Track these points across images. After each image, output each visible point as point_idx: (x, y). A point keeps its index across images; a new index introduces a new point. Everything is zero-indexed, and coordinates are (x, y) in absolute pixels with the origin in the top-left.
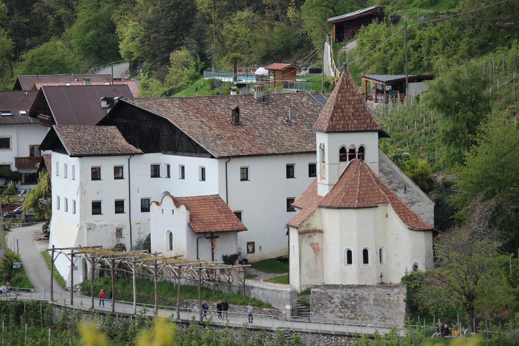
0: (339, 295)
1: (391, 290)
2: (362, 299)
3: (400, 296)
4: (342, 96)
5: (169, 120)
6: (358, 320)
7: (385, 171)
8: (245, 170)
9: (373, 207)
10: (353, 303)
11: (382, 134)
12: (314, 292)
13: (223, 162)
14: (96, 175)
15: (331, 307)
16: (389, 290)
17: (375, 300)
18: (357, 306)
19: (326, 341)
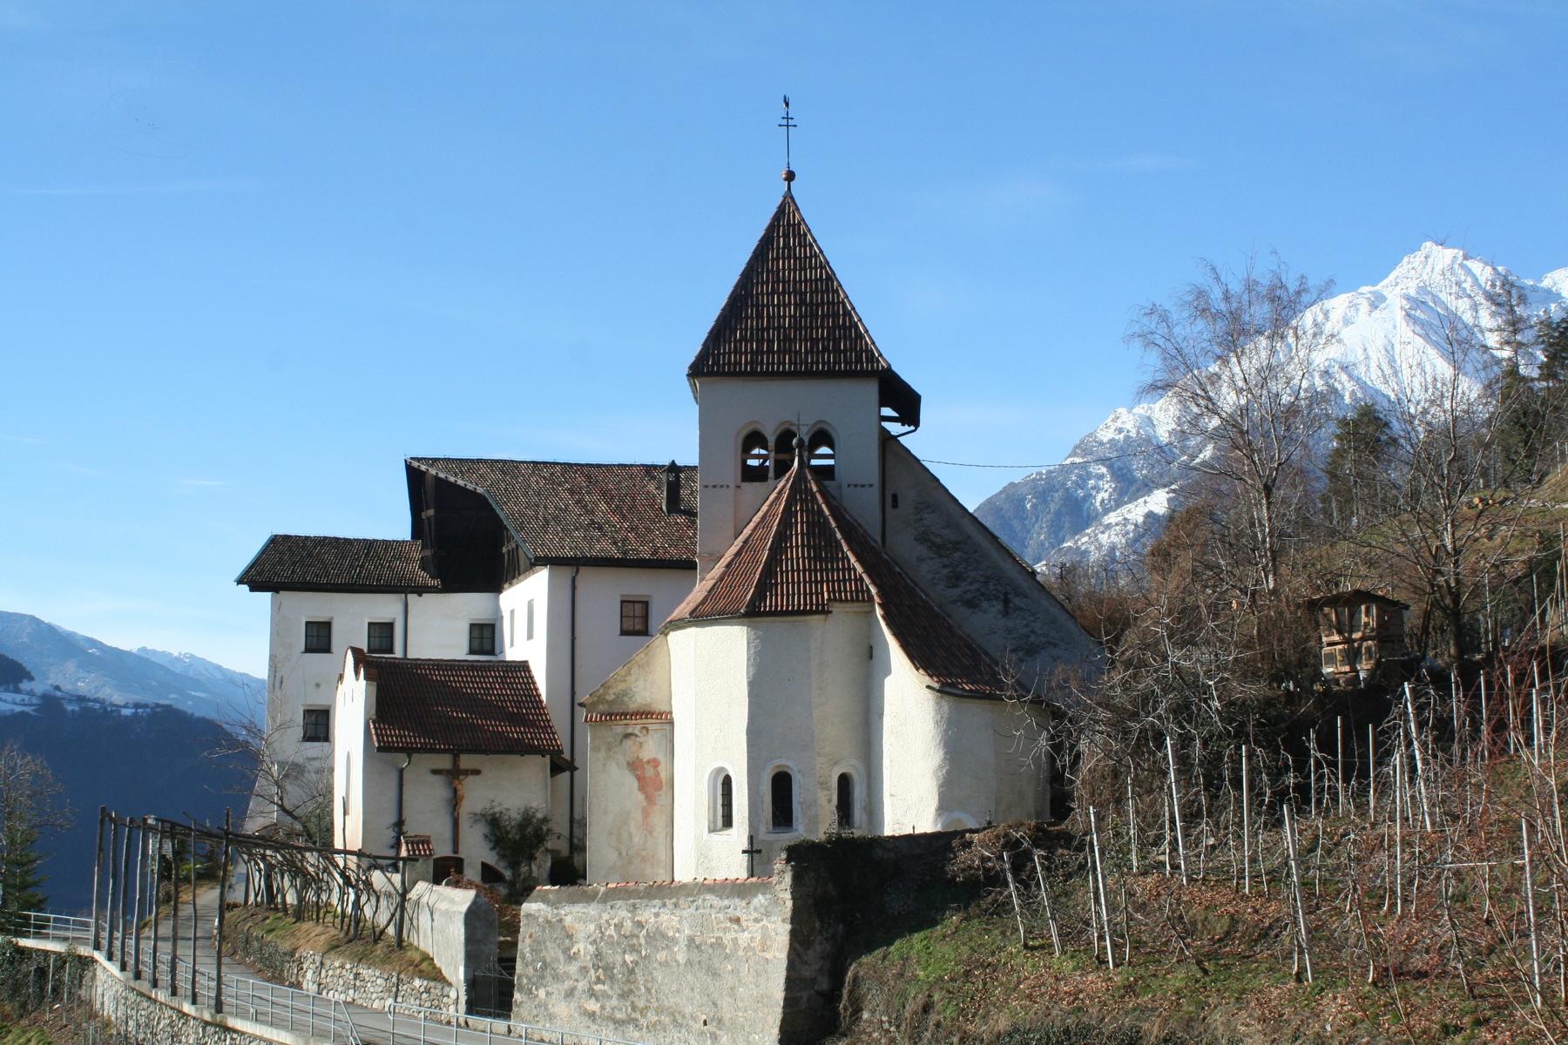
1: (744, 903)
7: (938, 541)
8: (638, 609)
10: (628, 958)
12: (528, 916)
13: (566, 573)
14: (319, 638)
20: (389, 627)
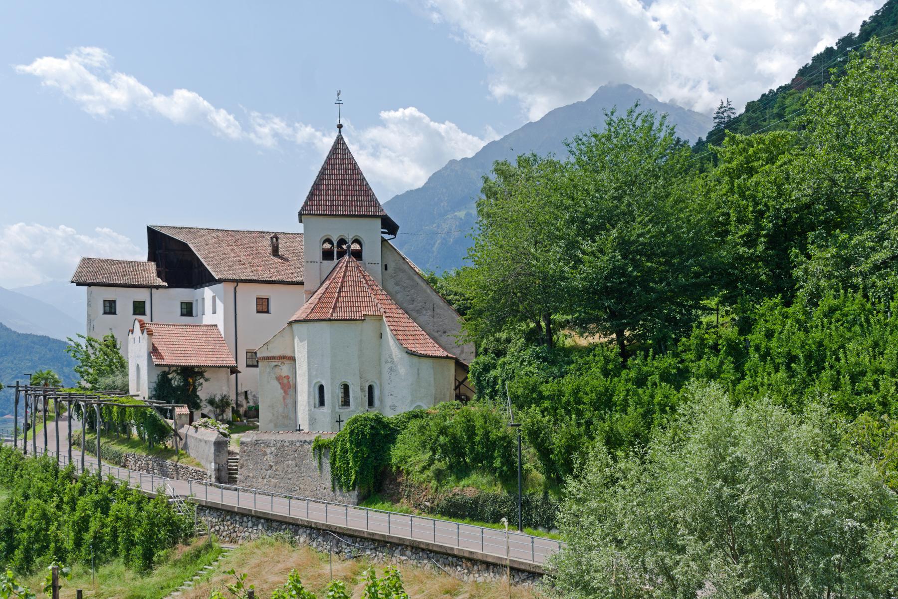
5: (191, 246)
20: (143, 303)
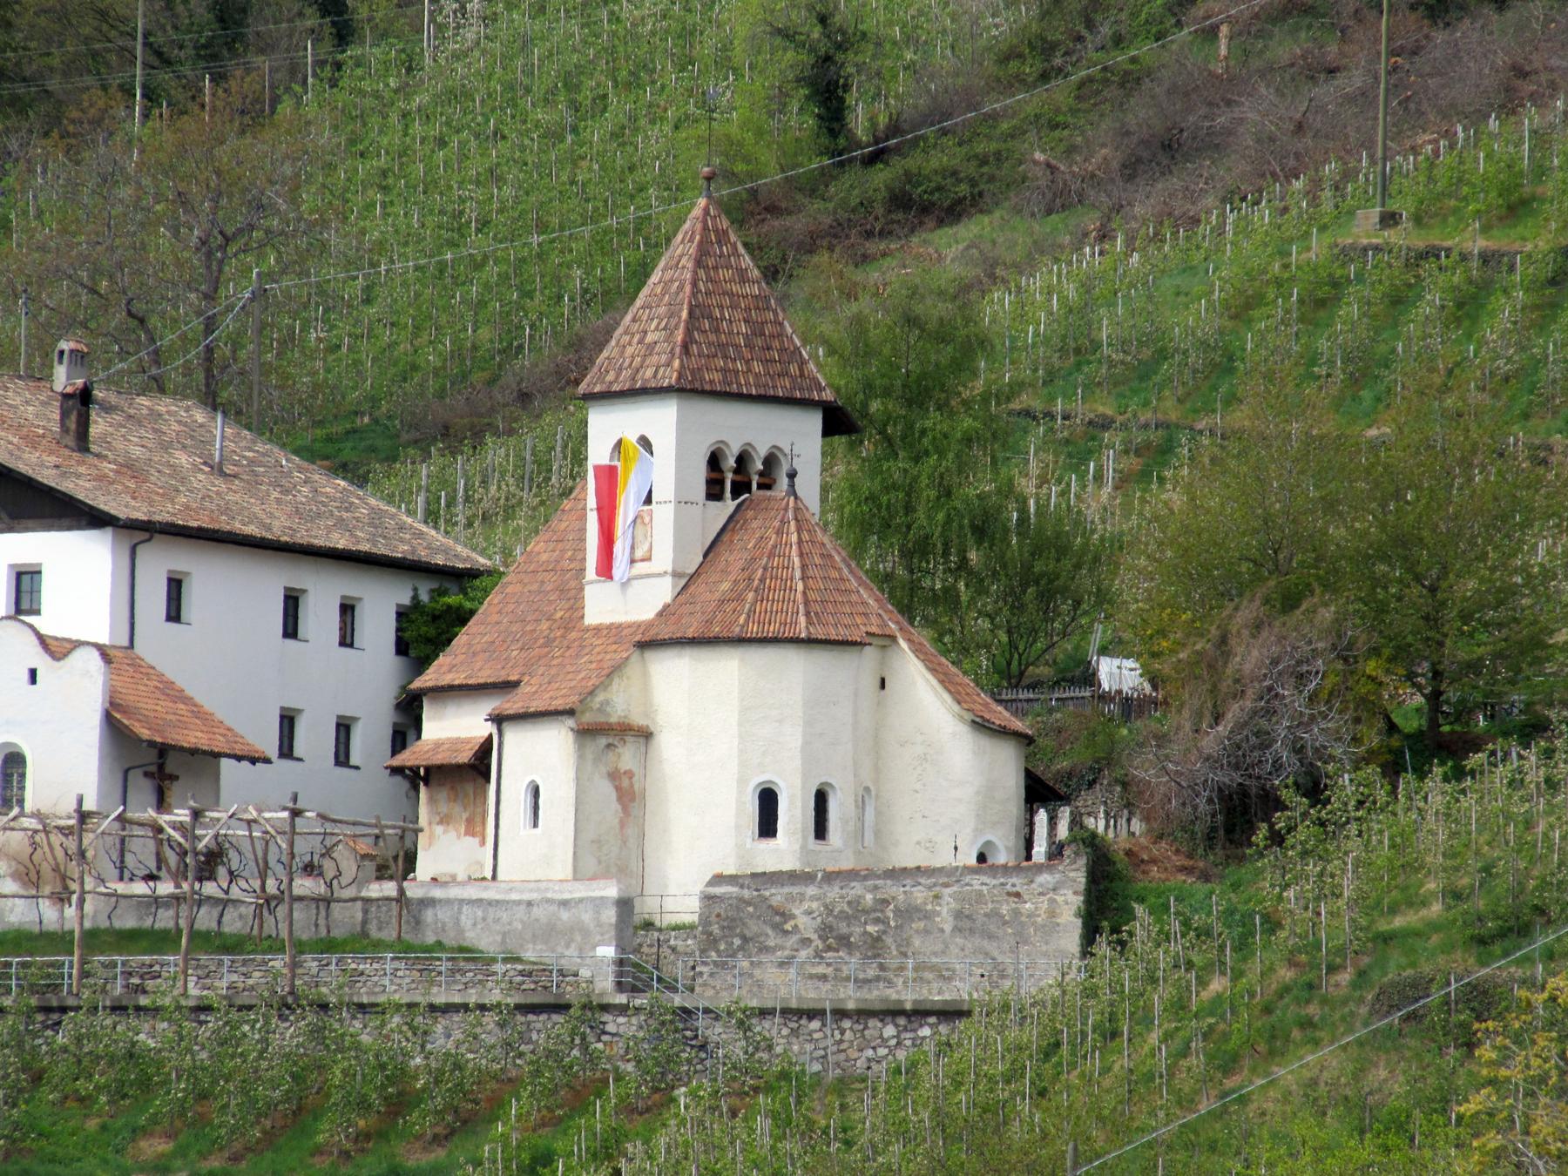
0: (815, 905)
2: (908, 913)
3: (1060, 899)
4: (709, 279)
6: (890, 983)
9: (854, 644)
11: (837, 422)
15: (782, 948)
16: (1014, 880)
17: (958, 915)
18: (889, 940)
19: (816, 1036)
